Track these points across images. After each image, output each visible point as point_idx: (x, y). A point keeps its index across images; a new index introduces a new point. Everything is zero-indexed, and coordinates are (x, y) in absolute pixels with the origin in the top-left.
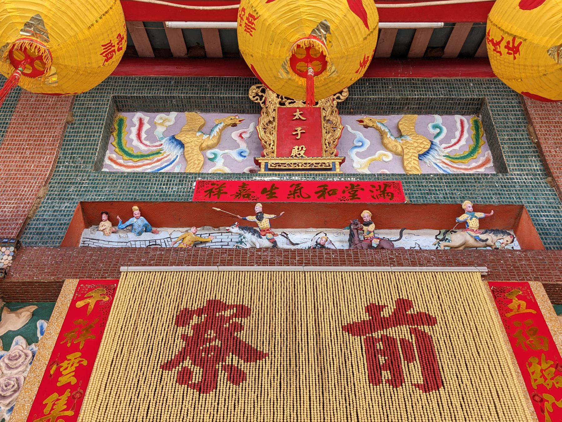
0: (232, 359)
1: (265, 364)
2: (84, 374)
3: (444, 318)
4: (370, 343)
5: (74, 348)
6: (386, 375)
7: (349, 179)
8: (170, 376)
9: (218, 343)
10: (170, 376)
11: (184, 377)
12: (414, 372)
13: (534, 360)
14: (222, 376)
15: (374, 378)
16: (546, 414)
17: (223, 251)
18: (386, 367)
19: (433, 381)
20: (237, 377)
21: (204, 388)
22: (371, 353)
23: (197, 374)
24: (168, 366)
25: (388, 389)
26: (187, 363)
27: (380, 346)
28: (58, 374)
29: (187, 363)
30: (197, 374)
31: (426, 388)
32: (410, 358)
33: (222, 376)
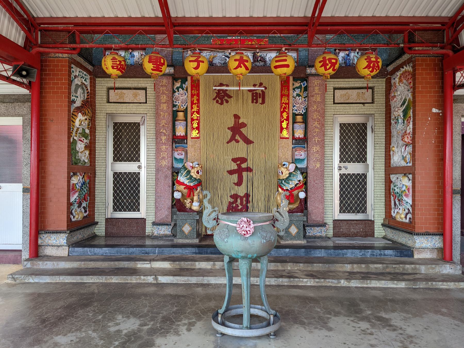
0: (226, 98)
1: (232, 99)
2: (198, 100)
3: (269, 88)
4: (253, 94)
5: (195, 95)
6: (255, 101)
7: (317, 91)
8: (215, 101)
9: (223, 94)
10: (215, 101)
11: (217, 102)
12: (260, 100)
13: (284, 97)
14: (224, 101)
15: (253, 102)
16: (12, 77)
17: (390, 132)
18: (255, 99)
19: (263, 102)
20: (227, 102)
21: (222, 104)
22: (253, 96)
23: (220, 101)
24: (214, 99)
25: (255, 104)
26: (218, 99)
27: (255, 95)
28: (193, 100)
29: (218, 99)
30: (220, 101)
31: (261, 104)
32: (260, 98)
33: (224, 101)
